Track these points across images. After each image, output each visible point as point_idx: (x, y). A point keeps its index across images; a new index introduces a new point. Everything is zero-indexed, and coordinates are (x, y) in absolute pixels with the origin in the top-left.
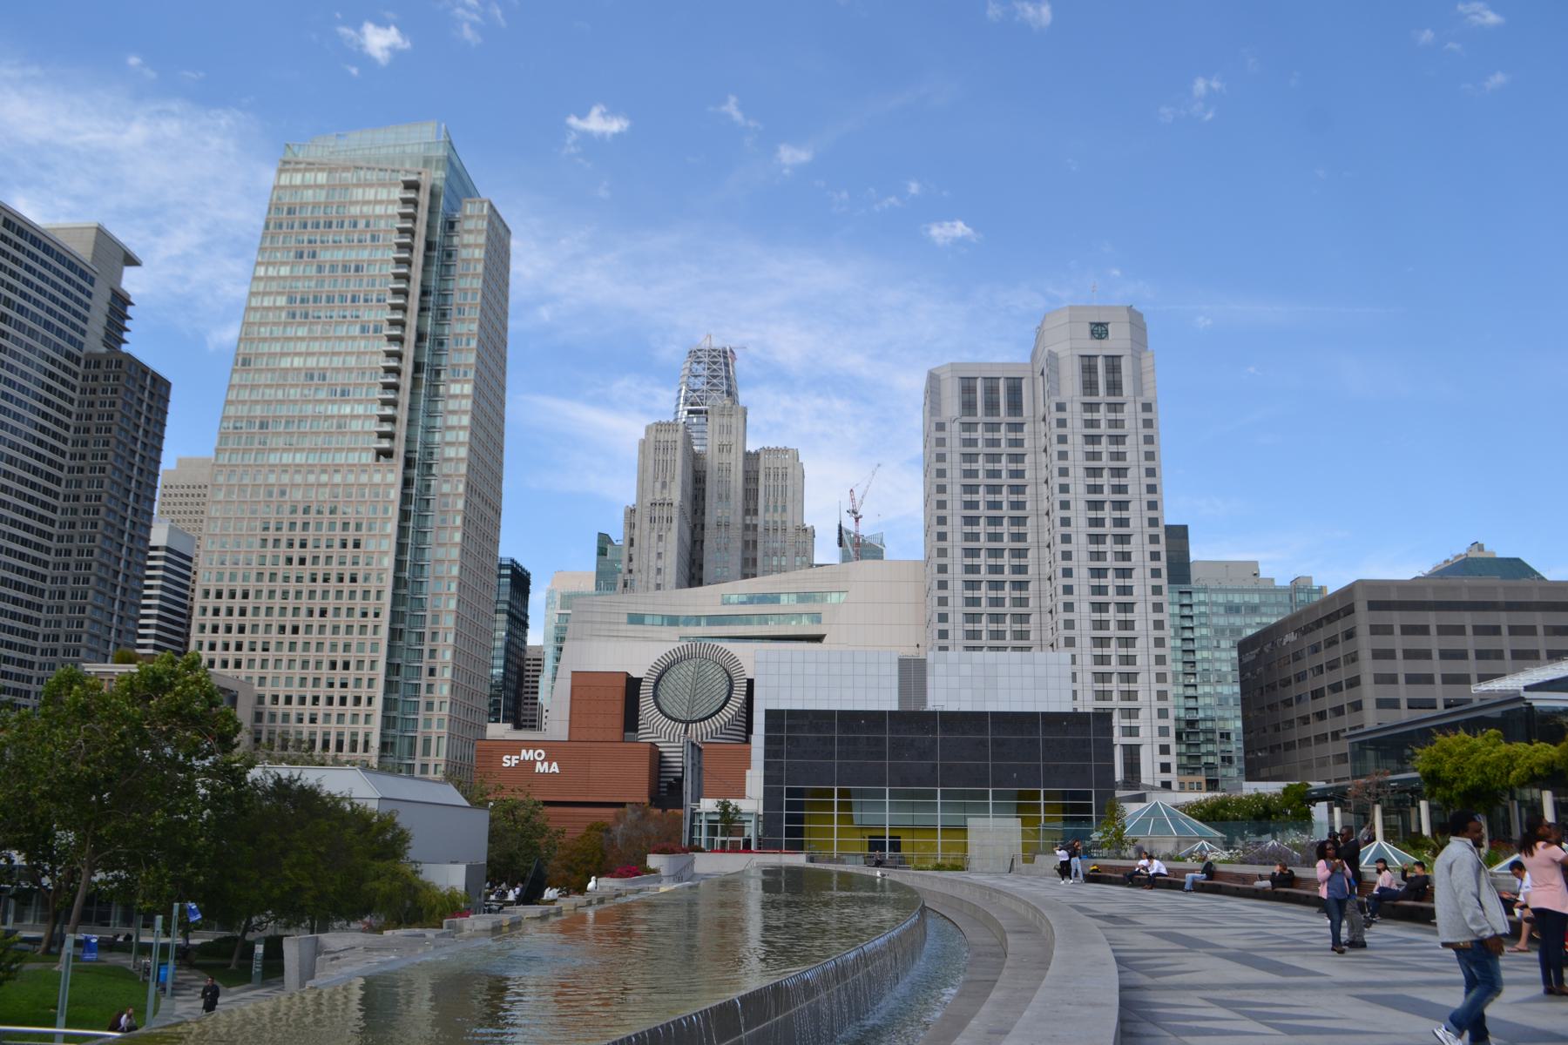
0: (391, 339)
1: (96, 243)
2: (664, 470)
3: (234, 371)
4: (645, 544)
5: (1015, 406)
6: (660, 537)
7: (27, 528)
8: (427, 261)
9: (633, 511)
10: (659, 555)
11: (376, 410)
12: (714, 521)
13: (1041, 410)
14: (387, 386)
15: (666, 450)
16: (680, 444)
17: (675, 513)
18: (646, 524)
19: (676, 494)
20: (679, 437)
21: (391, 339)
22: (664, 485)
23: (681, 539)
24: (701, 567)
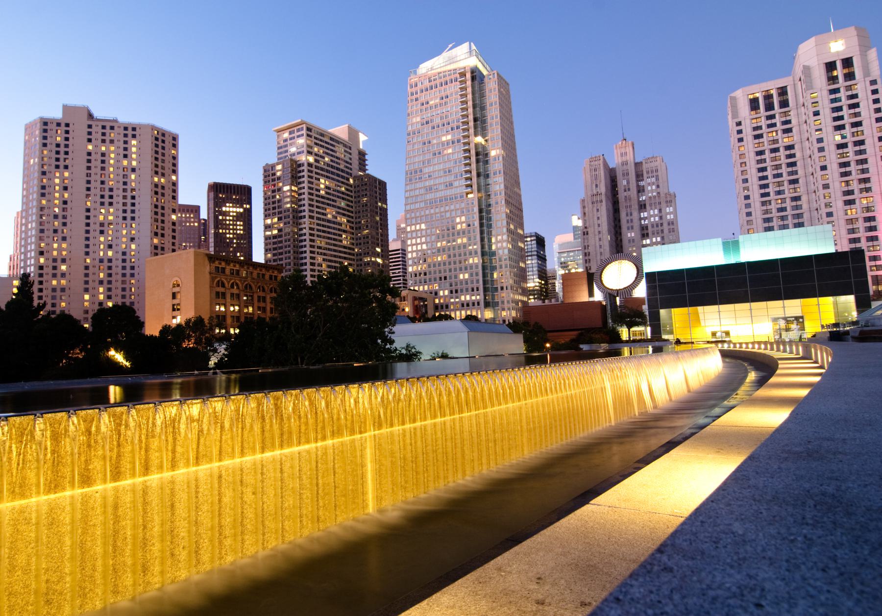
0: (467, 179)
1: (349, 133)
2: (596, 179)
3: (406, 185)
4: (591, 215)
5: (784, 104)
6: (598, 210)
7: (345, 253)
8: (478, 161)
9: (583, 201)
10: (598, 218)
11: (464, 169)
12: (623, 188)
13: (801, 100)
14: (466, 165)
15: (595, 170)
16: (602, 168)
17: (603, 198)
18: (590, 205)
19: (602, 189)
20: (601, 162)
21: (467, 179)
22: (597, 186)
23: (608, 210)
24: (619, 221)
